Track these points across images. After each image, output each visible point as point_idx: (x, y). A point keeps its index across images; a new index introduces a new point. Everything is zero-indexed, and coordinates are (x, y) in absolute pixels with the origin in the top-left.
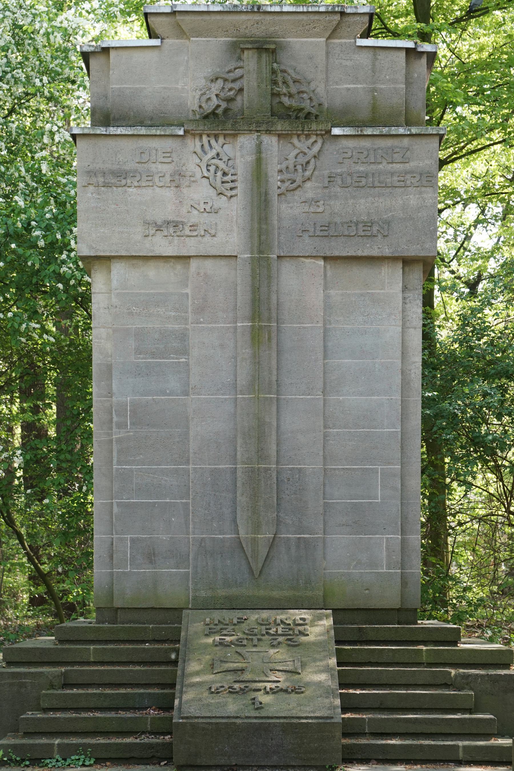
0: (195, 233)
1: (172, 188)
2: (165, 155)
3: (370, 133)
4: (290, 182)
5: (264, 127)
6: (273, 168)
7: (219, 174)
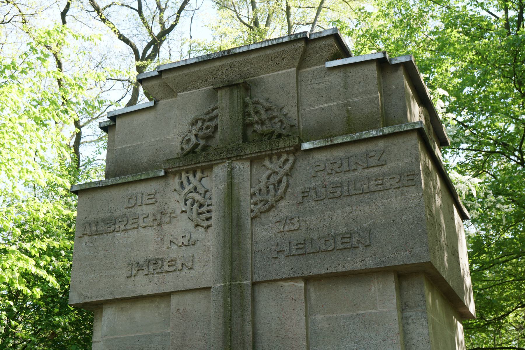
0: (173, 268)
1: (155, 227)
2: (149, 197)
3: (340, 141)
4: (263, 203)
5: (234, 154)
6: (244, 193)
7: (196, 206)
